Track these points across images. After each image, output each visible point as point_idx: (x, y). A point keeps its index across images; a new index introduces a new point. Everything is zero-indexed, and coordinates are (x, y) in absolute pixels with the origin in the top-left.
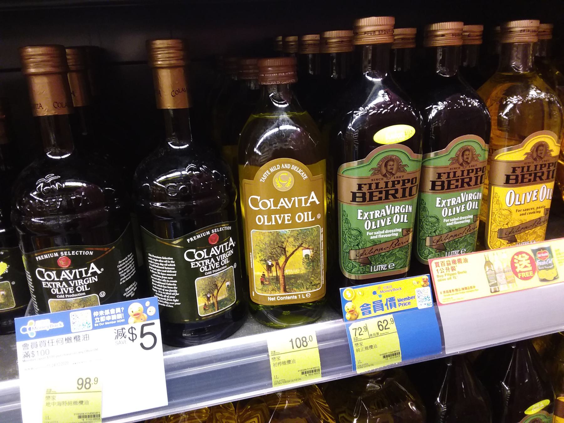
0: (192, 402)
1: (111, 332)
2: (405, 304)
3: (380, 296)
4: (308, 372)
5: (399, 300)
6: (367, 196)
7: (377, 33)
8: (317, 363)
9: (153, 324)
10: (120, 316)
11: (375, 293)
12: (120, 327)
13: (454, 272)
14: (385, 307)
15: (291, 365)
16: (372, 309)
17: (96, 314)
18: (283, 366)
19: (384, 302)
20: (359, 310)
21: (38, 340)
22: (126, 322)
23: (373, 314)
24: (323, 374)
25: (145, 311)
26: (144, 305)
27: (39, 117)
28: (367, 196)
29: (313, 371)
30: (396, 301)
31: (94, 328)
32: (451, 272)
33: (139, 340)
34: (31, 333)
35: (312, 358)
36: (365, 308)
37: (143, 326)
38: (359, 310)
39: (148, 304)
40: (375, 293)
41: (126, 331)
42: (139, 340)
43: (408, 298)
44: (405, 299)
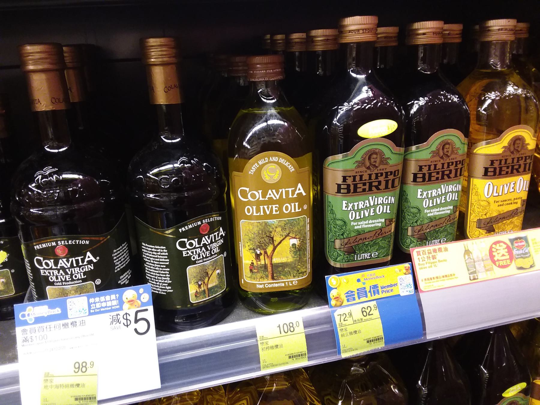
0: (184, 385)
1: (106, 317)
2: (388, 291)
3: (364, 284)
4: (295, 356)
5: (382, 288)
6: (352, 188)
7: (361, 32)
8: (303, 348)
9: (147, 310)
10: (115, 303)
11: (359, 280)
12: (115, 313)
13: (435, 260)
14: (369, 294)
15: (279, 349)
16: (356, 296)
17: (92, 300)
18: (271, 351)
19: (368, 289)
20: (343, 297)
21: (37, 326)
22: (121, 309)
23: (357, 301)
24: (310, 359)
25: (139, 298)
26: (137, 292)
27: (38, 112)
28: (352, 188)
29: (300, 356)
30: (380, 288)
31: (90, 314)
32: (432, 260)
33: (133, 326)
34: (30, 319)
35: (299, 342)
36: (350, 295)
37: (137, 312)
38: (343, 297)
39: (141, 291)
40: (359, 280)
41: (121, 317)
42: (133, 326)
43: (391, 286)
44: (388, 286)
